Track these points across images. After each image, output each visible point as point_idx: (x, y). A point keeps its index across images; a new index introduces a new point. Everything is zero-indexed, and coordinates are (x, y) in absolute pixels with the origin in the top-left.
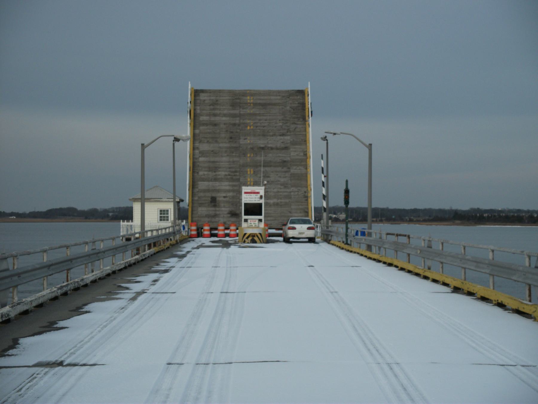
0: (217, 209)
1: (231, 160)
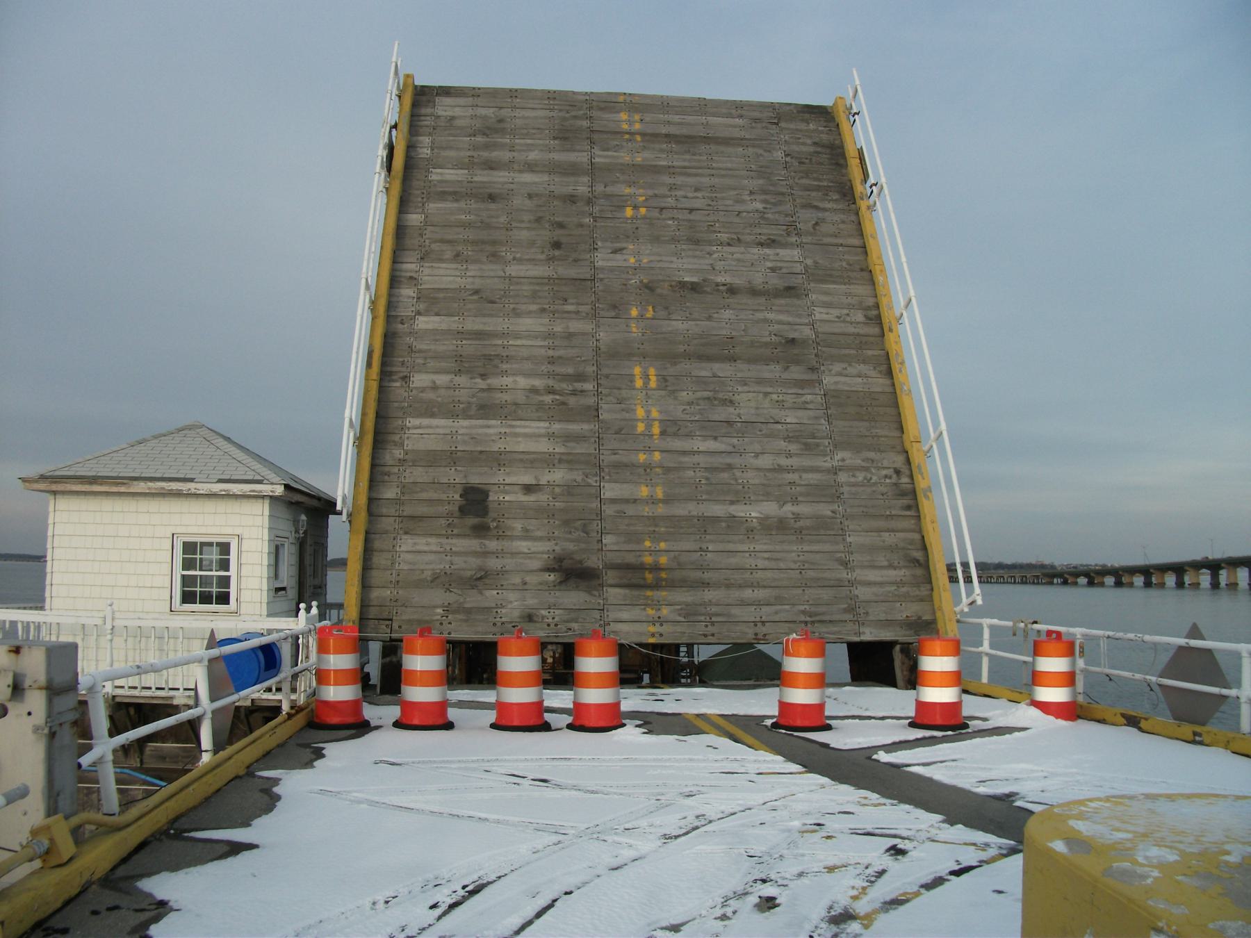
0: (492, 545)
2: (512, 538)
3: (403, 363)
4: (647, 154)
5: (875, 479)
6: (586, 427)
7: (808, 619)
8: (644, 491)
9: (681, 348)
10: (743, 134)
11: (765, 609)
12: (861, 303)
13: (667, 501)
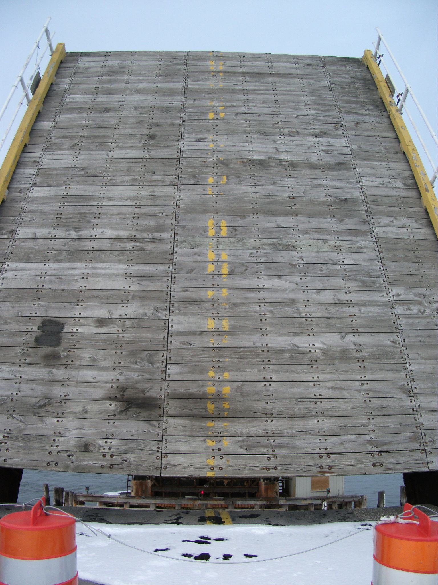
0: (60, 373)
1: (146, 192)
2: (80, 367)
3: (13, 221)
4: (227, 83)
5: (428, 312)
6: (160, 268)
7: (375, 449)
8: (210, 324)
9: (250, 206)
10: (298, 72)
11: (331, 440)
12: (399, 174)
13: (232, 333)
